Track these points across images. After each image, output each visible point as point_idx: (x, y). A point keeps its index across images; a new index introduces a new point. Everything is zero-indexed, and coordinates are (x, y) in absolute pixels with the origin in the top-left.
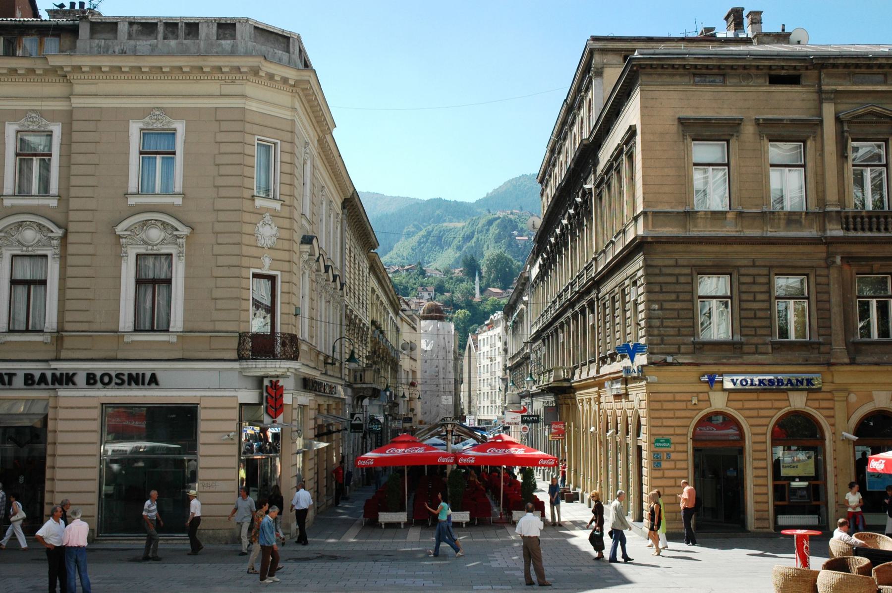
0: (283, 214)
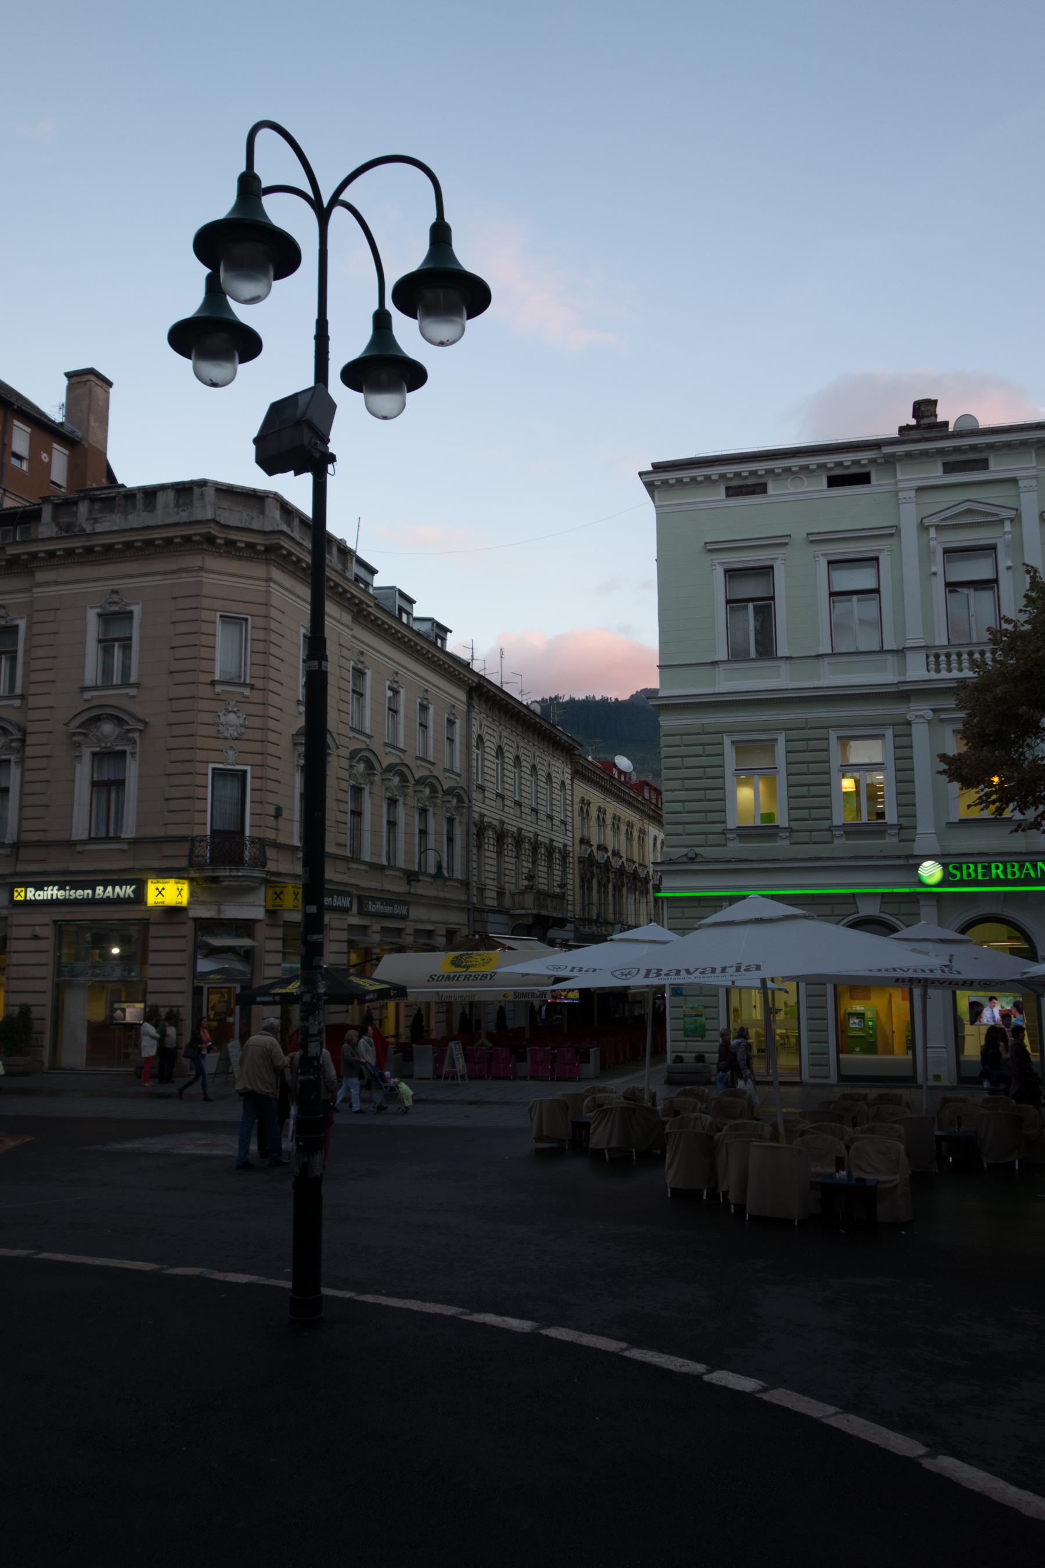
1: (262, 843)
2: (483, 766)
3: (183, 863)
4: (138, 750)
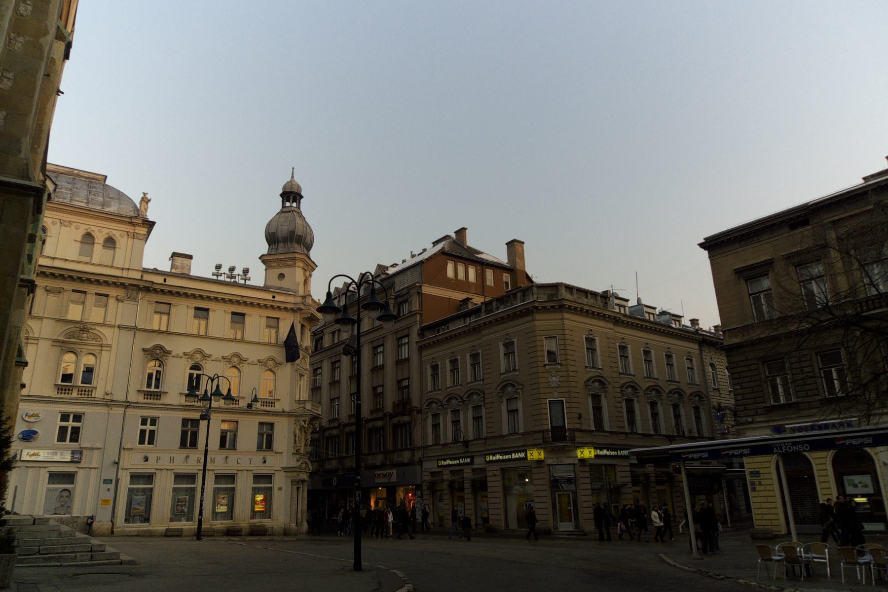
0: (562, 370)
1: (573, 430)
2: (717, 378)
3: (541, 441)
4: (521, 396)
